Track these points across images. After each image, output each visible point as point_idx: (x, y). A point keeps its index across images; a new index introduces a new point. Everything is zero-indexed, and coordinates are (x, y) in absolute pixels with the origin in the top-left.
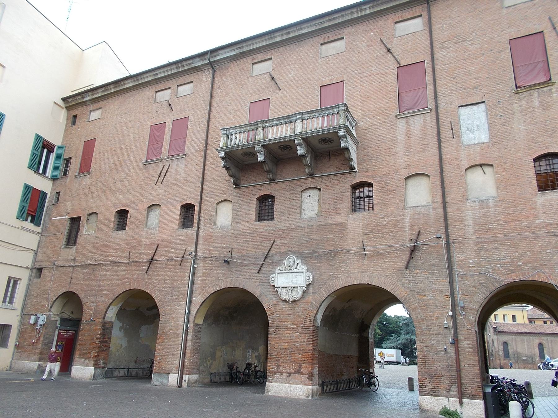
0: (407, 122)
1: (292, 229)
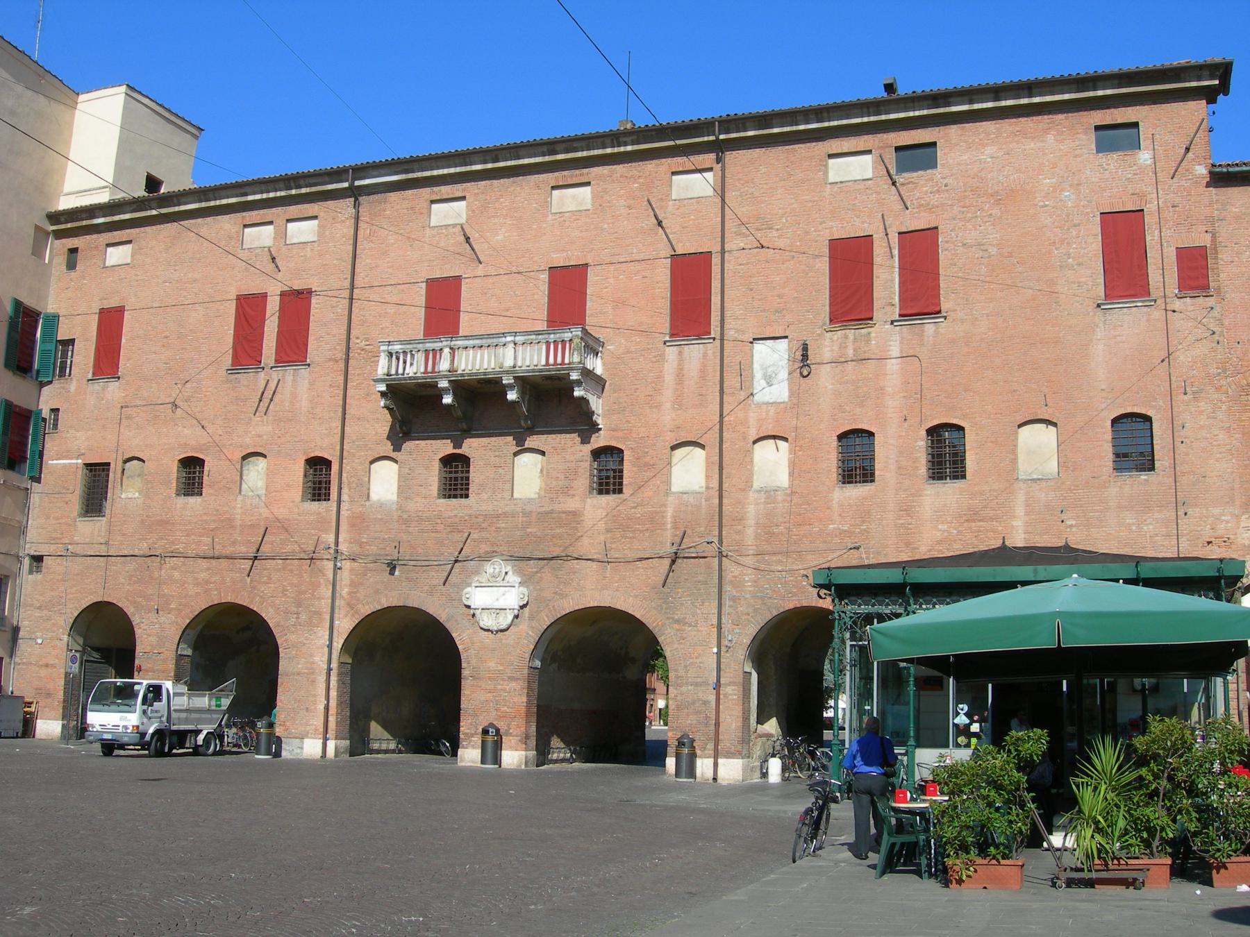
0: (680, 353)
1: (498, 516)
